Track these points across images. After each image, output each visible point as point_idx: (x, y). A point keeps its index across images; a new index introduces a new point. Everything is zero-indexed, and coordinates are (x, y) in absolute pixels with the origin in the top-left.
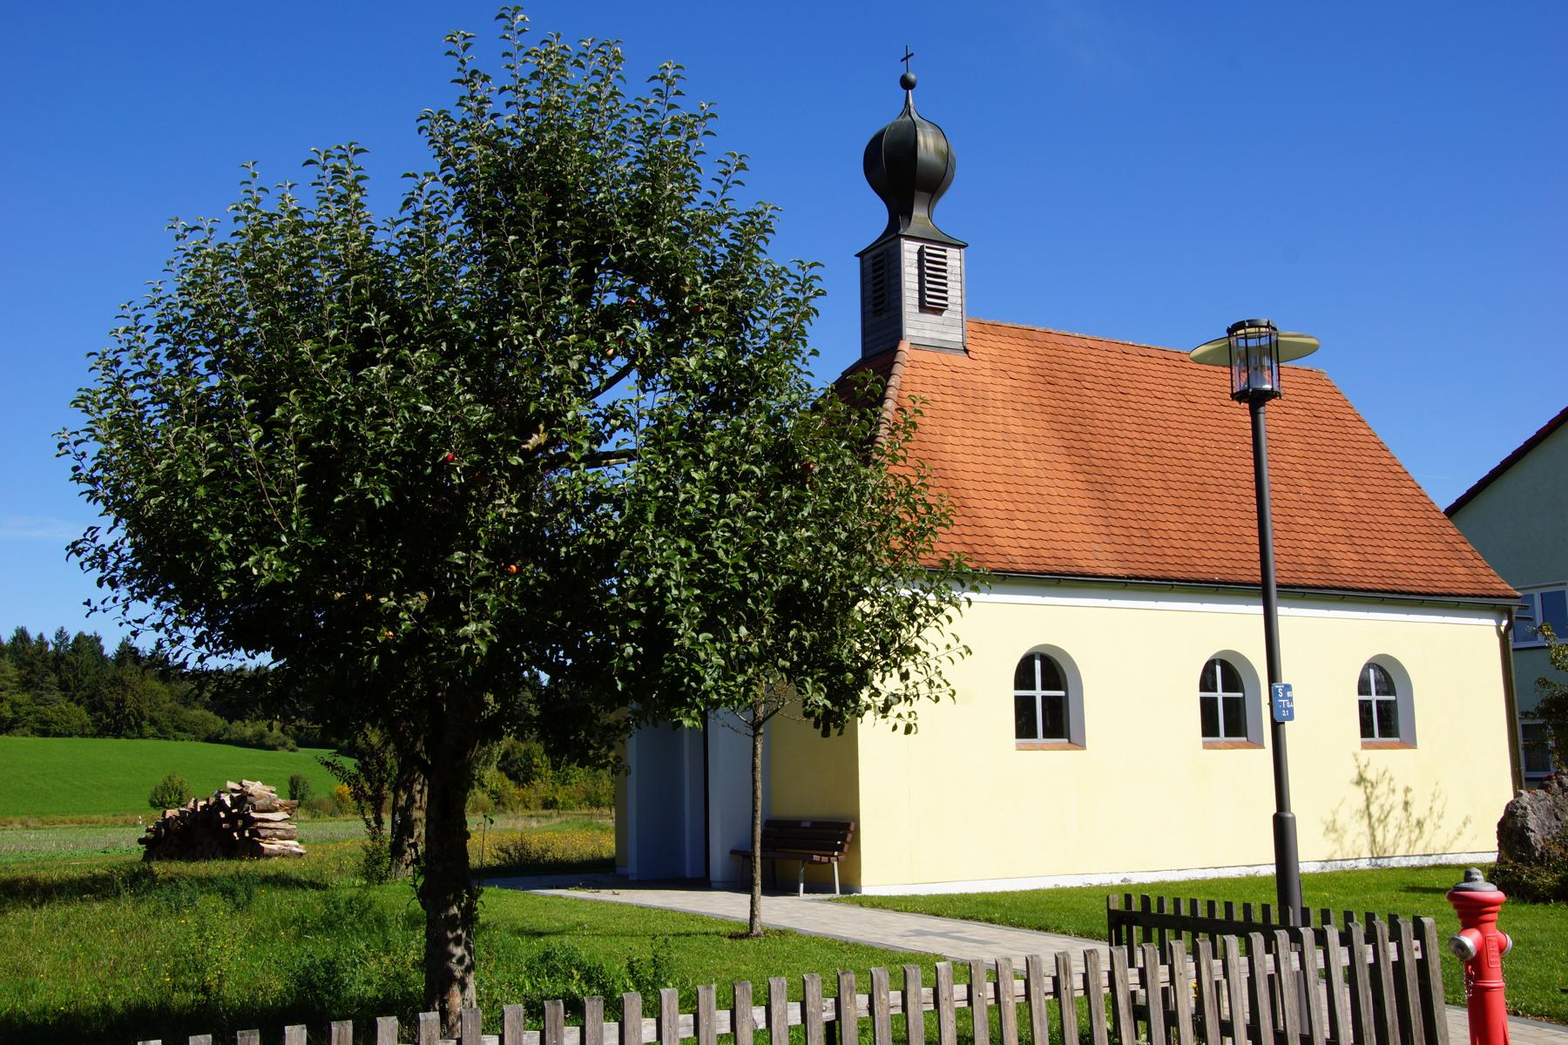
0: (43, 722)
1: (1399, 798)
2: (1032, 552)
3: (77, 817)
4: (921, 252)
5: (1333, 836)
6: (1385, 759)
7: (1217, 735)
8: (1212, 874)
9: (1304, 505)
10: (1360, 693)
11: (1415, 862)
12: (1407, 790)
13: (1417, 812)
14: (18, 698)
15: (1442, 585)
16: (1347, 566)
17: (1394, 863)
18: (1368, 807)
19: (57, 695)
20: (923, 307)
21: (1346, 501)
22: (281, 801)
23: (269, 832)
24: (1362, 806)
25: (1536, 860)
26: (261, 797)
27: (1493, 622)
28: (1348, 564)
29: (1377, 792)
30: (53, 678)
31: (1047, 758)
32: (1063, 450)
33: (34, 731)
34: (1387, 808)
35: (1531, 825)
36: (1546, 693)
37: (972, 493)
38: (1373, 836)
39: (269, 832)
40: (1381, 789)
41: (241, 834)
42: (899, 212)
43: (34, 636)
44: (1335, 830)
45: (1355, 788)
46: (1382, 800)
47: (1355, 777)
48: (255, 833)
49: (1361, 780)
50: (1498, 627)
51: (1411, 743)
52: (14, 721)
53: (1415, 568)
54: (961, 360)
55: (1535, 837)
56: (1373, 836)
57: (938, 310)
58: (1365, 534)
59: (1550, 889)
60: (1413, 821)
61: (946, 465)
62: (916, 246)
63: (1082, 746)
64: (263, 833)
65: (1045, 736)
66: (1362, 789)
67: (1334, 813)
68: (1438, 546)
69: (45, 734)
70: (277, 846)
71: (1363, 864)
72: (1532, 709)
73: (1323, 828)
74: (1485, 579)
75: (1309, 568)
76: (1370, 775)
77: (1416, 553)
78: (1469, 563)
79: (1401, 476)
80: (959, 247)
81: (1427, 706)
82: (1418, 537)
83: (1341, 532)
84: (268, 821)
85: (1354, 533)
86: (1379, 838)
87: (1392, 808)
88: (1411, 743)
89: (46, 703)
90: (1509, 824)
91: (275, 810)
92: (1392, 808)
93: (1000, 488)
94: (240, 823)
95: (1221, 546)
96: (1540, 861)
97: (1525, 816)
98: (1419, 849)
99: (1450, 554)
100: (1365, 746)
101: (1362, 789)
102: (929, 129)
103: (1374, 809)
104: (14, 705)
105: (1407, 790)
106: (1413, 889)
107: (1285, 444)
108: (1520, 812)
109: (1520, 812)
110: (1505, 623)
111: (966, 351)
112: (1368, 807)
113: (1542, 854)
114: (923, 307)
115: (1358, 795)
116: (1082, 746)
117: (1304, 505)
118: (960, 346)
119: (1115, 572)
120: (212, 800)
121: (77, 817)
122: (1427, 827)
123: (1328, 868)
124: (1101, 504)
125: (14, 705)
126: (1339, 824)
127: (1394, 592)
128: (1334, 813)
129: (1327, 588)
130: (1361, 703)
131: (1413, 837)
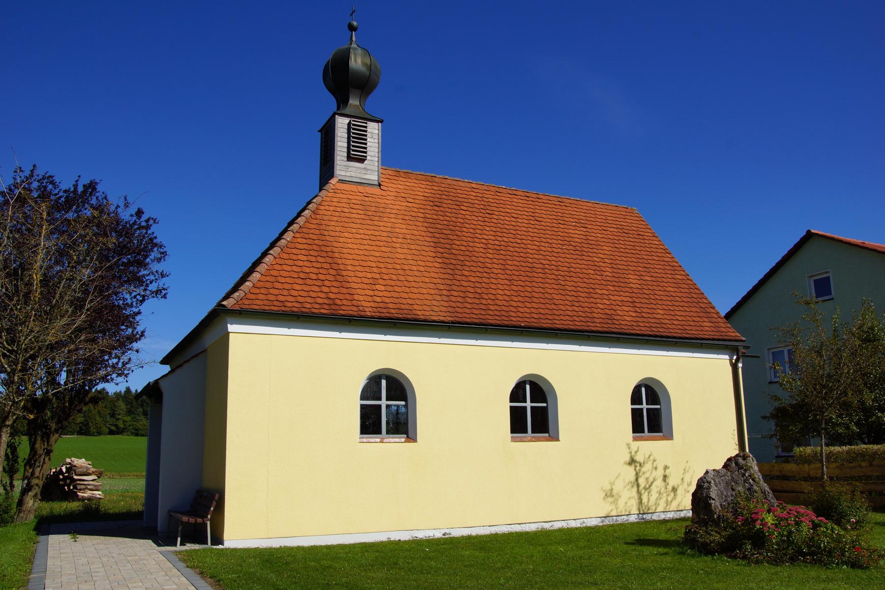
0: (136, 430)
1: (660, 472)
2: (382, 305)
3: (135, 474)
4: (349, 124)
5: (610, 500)
6: (651, 448)
7: (526, 432)
8: (517, 529)
9: (605, 283)
10: (633, 403)
11: (670, 516)
12: (666, 468)
13: (672, 482)
14: (125, 418)
15: (693, 332)
16: (626, 318)
17: (655, 517)
18: (637, 479)
19: (142, 417)
20: (350, 158)
21: (636, 281)
22: (93, 470)
23: (83, 487)
24: (633, 478)
25: (714, 521)
26: (81, 467)
27: (727, 357)
28: (628, 318)
29: (643, 469)
30: (141, 410)
31: (534, 449)
32: (432, 244)
33: (132, 434)
34: (651, 479)
35: (713, 495)
36: (777, 404)
37: (349, 268)
38: (640, 499)
39: (83, 487)
40: (647, 467)
41: (69, 488)
42: (342, 102)
43: (133, 391)
44: (612, 496)
45: (628, 467)
46: (647, 475)
47: (628, 459)
48: (75, 487)
49: (632, 462)
50: (731, 360)
51: (669, 437)
52: (124, 429)
53: (675, 322)
54: (377, 191)
55: (716, 503)
56: (640, 499)
57: (362, 160)
58: (644, 301)
59: (719, 544)
60: (670, 488)
61: (336, 250)
62: (346, 121)
63: (557, 439)
64: (79, 487)
65: (387, 433)
66: (633, 467)
67: (612, 484)
68: (694, 309)
69: (137, 435)
70: (87, 494)
71: (633, 519)
72: (768, 415)
73: (603, 495)
74: (723, 330)
75: (598, 321)
76: (639, 458)
77: (678, 313)
78: (714, 320)
79: (676, 268)
80: (377, 122)
81: (681, 412)
82: (681, 304)
83: (628, 299)
84: (83, 480)
85: (636, 300)
86: (645, 500)
87: (654, 480)
88: (669, 437)
89: (137, 421)
90: (699, 495)
91: (90, 474)
92: (654, 480)
93: (373, 265)
94: (68, 481)
95: (535, 305)
96: (716, 523)
97: (709, 488)
98: (674, 506)
99: (702, 314)
100: (635, 439)
101: (633, 467)
102: (360, 51)
103: (642, 481)
104: (124, 422)
105: (666, 468)
106: (643, 542)
107: (599, 247)
108: (706, 485)
109: (706, 485)
110: (735, 357)
111: (380, 185)
112: (637, 479)
113: (719, 516)
114: (350, 158)
115: (630, 472)
116: (557, 439)
117: (605, 283)
118: (376, 183)
119: (442, 318)
120: (58, 469)
121: (135, 474)
122: (679, 492)
123: (607, 522)
124: (450, 277)
125: (124, 422)
126: (615, 492)
127: (656, 336)
128: (612, 484)
129: (607, 333)
130: (634, 411)
131: (670, 499)
